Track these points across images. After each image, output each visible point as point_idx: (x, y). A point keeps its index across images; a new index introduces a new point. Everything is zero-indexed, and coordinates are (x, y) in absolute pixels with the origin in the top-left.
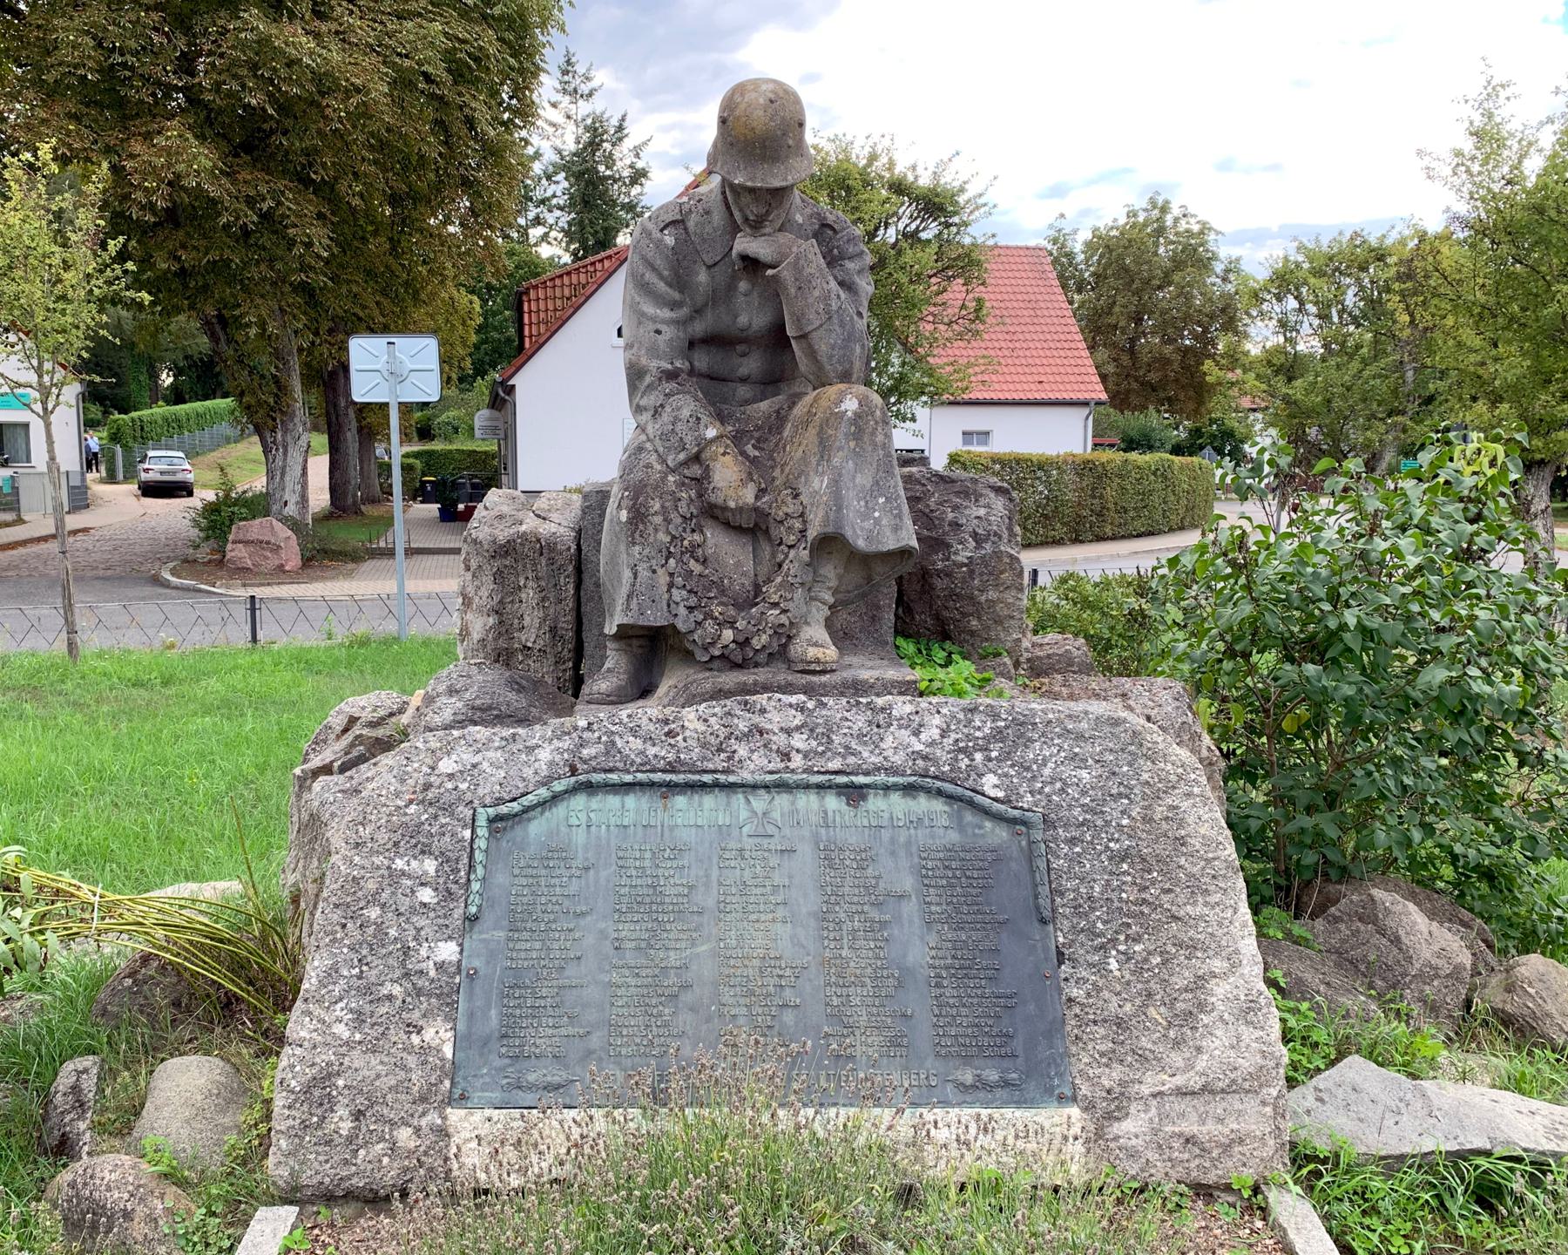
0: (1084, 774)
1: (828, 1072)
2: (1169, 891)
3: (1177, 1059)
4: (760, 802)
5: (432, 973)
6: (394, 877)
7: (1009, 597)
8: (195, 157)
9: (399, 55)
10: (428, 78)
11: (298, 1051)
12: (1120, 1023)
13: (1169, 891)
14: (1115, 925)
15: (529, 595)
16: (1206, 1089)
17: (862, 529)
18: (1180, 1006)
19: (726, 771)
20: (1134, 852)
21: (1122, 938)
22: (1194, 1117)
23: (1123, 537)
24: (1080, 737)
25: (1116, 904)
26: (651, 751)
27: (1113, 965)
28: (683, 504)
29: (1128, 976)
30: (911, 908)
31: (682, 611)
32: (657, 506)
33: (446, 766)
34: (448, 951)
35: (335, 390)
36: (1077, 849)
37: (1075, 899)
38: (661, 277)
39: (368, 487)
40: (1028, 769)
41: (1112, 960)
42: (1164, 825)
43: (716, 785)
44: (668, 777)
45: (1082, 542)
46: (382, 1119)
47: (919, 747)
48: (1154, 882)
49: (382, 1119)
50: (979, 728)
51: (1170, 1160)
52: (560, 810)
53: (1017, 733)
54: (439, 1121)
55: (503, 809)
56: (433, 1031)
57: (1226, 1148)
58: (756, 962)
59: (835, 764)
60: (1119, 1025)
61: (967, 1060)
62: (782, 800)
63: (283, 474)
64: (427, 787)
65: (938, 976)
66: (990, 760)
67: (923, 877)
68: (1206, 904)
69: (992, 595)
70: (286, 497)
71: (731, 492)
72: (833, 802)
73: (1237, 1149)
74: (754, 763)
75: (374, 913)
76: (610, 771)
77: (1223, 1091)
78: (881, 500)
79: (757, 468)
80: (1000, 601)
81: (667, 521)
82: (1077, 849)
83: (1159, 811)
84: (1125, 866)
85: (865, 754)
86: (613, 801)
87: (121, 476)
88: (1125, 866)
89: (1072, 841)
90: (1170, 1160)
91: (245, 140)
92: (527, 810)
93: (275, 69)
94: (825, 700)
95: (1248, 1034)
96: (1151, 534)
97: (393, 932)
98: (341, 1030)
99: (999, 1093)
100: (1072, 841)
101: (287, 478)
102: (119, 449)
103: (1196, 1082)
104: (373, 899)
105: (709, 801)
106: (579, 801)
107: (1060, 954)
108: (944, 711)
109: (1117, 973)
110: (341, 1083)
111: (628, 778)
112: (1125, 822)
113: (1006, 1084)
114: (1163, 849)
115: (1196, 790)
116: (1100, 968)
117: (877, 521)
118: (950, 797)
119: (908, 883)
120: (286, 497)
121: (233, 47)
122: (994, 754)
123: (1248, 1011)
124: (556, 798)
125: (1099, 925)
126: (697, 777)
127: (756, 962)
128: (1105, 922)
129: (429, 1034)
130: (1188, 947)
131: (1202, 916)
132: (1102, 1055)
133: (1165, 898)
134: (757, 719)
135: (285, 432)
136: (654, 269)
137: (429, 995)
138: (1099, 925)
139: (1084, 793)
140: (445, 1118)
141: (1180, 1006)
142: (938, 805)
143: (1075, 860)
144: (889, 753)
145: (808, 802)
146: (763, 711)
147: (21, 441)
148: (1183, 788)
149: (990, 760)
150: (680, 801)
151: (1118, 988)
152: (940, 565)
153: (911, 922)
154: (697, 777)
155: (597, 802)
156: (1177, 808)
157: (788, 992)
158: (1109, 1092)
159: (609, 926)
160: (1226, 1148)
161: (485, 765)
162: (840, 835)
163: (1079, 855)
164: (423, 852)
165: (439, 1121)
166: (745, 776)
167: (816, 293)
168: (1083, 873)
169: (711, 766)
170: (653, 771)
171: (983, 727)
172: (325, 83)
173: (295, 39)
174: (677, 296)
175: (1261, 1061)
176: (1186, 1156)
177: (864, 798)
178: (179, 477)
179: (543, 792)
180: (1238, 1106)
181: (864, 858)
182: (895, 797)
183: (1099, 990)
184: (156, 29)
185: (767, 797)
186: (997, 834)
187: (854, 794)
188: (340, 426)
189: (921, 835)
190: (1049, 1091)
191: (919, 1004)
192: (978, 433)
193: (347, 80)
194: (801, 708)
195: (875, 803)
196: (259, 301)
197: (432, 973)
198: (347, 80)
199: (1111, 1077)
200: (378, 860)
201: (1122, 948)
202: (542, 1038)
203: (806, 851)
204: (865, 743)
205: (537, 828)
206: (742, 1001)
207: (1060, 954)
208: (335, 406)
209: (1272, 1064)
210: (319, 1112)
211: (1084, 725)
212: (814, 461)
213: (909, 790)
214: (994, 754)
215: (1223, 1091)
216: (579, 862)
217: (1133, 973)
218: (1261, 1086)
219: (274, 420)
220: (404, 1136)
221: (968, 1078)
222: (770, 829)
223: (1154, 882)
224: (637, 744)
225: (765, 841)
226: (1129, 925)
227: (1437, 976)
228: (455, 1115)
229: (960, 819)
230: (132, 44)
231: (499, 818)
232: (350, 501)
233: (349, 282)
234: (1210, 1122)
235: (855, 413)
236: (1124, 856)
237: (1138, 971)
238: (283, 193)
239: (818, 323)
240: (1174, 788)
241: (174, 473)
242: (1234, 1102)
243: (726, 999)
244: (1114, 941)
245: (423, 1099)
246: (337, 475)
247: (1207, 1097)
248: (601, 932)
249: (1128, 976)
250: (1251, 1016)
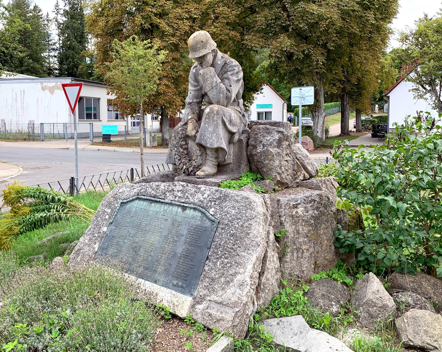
0: (233, 211)
1: (148, 274)
2: (240, 247)
3: (220, 293)
4: (166, 207)
7: (271, 162)
8: (287, 43)
9: (343, 6)
10: (354, 11)
12: (213, 280)
13: (240, 247)
14: (223, 253)
16: (221, 303)
17: (209, 142)
18: (228, 279)
19: (164, 199)
20: (235, 234)
21: (223, 257)
22: (216, 309)
24: (237, 201)
25: (226, 248)
26: (153, 192)
27: (218, 264)
28: (180, 135)
29: (220, 268)
30: (183, 238)
31: (177, 160)
32: (173, 135)
33: (121, 191)
35: (343, 100)
36: (223, 231)
37: (216, 244)
39: (358, 127)
40: (222, 208)
41: (219, 262)
42: (245, 229)
43: (159, 202)
47: (202, 199)
48: (237, 244)
50: (216, 196)
51: (203, 318)
52: (133, 203)
53: (225, 198)
55: (124, 201)
57: (218, 321)
58: (150, 244)
59: (183, 201)
60: (212, 280)
61: (177, 278)
62: (171, 207)
63: (317, 124)
64: (116, 194)
65: (180, 256)
66: (215, 204)
67: (189, 232)
68: (247, 253)
69: (267, 162)
70: (318, 130)
71: (190, 132)
72: (180, 210)
73: (221, 322)
74: (169, 198)
77: (225, 305)
78: (215, 134)
80: (269, 164)
81: (175, 138)
82: (223, 231)
83: (246, 224)
84: (232, 238)
85: (191, 199)
86: (142, 202)
87: (296, 125)
88: (232, 238)
89: (222, 229)
90: (203, 318)
91: (301, 36)
92: (128, 202)
93: (307, 17)
94: (188, 184)
95: (238, 291)
98: (87, 241)
99: (180, 289)
100: (222, 229)
101: (318, 125)
102: (296, 117)
103: (220, 300)
105: (158, 205)
106: (137, 201)
107: (208, 257)
108: (211, 190)
109: (218, 266)
111: (145, 197)
112: (237, 226)
113: (182, 287)
114: (242, 235)
115: (258, 220)
116: (215, 264)
117: (213, 140)
118: (203, 213)
119: (185, 232)
120: (318, 130)
121: (297, 13)
122: (217, 203)
123: (241, 285)
124: (133, 200)
125: (219, 252)
127: (150, 244)
128: (221, 252)
130: (238, 264)
131: (244, 256)
132: (205, 286)
133: (238, 249)
134: (174, 187)
135: (319, 112)
138: (219, 252)
139: (231, 216)
141: (228, 279)
142: (199, 214)
143: (221, 234)
144: (195, 199)
145: (175, 209)
146: (176, 186)
147: (270, 116)
148: (256, 219)
149: (215, 204)
150: (153, 204)
151: (217, 270)
152: (254, 153)
153: (182, 242)
156: (251, 224)
157: (152, 253)
158: (201, 296)
160: (218, 321)
162: (177, 217)
163: (223, 232)
166: (166, 201)
167: (209, 82)
168: (221, 238)
169: (161, 197)
170: (151, 197)
171: (218, 195)
172: (321, 18)
173: (313, 8)
174: (196, 84)
175: (237, 300)
176: (207, 319)
177: (186, 210)
178: (309, 125)
179: (131, 199)
180: (227, 310)
181: (180, 224)
182: (192, 210)
183: (212, 269)
184: (280, 13)
185: (177, 208)
186: (208, 223)
187: (184, 208)
188: (344, 110)
189: (193, 221)
190: (190, 292)
191: (174, 263)
193: (326, 16)
194: (183, 186)
195: (188, 211)
196: (306, 78)
198: (326, 16)
199: (203, 292)
201: (222, 260)
203: (170, 220)
204: (191, 196)
205: (128, 206)
206: (144, 252)
207: (208, 257)
208: (343, 104)
209: (240, 302)
211: (239, 198)
213: (195, 209)
214: (217, 203)
215: (225, 305)
216: (131, 215)
217: (222, 267)
218: (234, 307)
219: (316, 109)
221: (175, 283)
222: (166, 214)
223: (237, 244)
224: (150, 190)
225: (164, 217)
226: (226, 254)
227: (375, 306)
229: (202, 218)
230: (274, 18)
231: (122, 203)
232: (346, 131)
233: (335, 70)
234: (219, 312)
235: (208, 112)
236: (232, 235)
237: (223, 267)
238: (310, 48)
239: (209, 90)
240: (253, 219)
241: (308, 123)
242: (227, 309)
244: (221, 257)
246: (343, 124)
247: (221, 305)
249: (220, 268)
250: (241, 287)
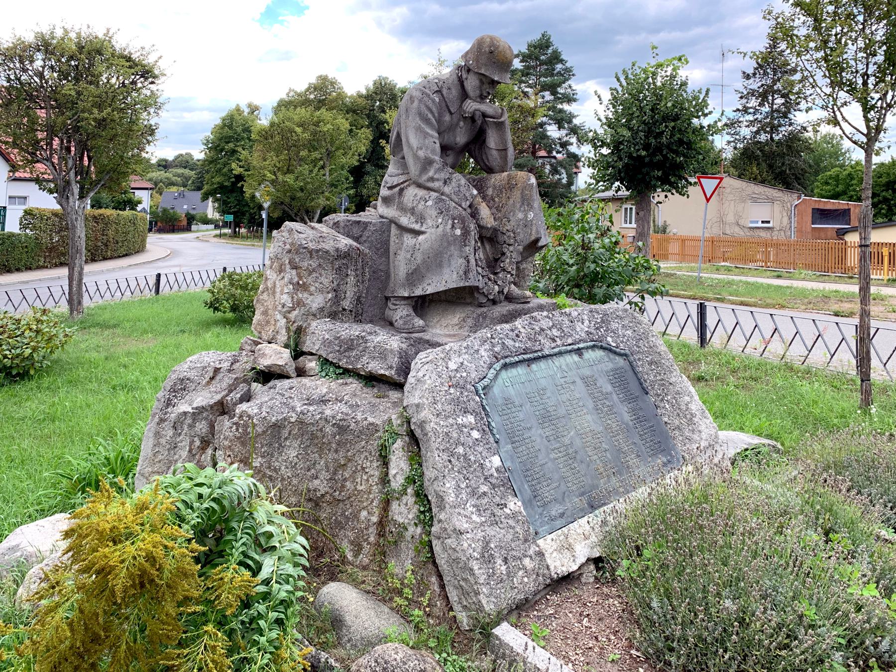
5: (495, 474)
6: (460, 427)
11: (469, 536)
15: (351, 280)
23: (116, 258)
33: (452, 366)
34: (496, 461)
38: (434, 116)
44: (525, 357)
45: (96, 261)
46: (515, 558)
49: (515, 558)
54: (537, 549)
56: (512, 503)
59: (570, 341)
75: (460, 450)
76: (506, 357)
79: (496, 209)
96: (126, 255)
97: (473, 458)
104: (458, 443)
110: (492, 546)
111: (516, 359)
126: (536, 354)
129: (511, 505)
136: (432, 112)
137: (499, 487)
140: (538, 546)
150: (534, 366)
154: (536, 354)
155: (513, 372)
159: (540, 431)
161: (465, 362)
164: (465, 412)
165: (537, 549)
187: (579, 352)
192: (19, 197)
197: (495, 474)
200: (451, 421)
202: (547, 493)
210: (490, 566)
212: (518, 205)
220: (527, 562)
228: (540, 542)
243: (590, 454)
245: (526, 540)
248: (540, 435)
